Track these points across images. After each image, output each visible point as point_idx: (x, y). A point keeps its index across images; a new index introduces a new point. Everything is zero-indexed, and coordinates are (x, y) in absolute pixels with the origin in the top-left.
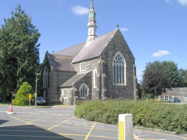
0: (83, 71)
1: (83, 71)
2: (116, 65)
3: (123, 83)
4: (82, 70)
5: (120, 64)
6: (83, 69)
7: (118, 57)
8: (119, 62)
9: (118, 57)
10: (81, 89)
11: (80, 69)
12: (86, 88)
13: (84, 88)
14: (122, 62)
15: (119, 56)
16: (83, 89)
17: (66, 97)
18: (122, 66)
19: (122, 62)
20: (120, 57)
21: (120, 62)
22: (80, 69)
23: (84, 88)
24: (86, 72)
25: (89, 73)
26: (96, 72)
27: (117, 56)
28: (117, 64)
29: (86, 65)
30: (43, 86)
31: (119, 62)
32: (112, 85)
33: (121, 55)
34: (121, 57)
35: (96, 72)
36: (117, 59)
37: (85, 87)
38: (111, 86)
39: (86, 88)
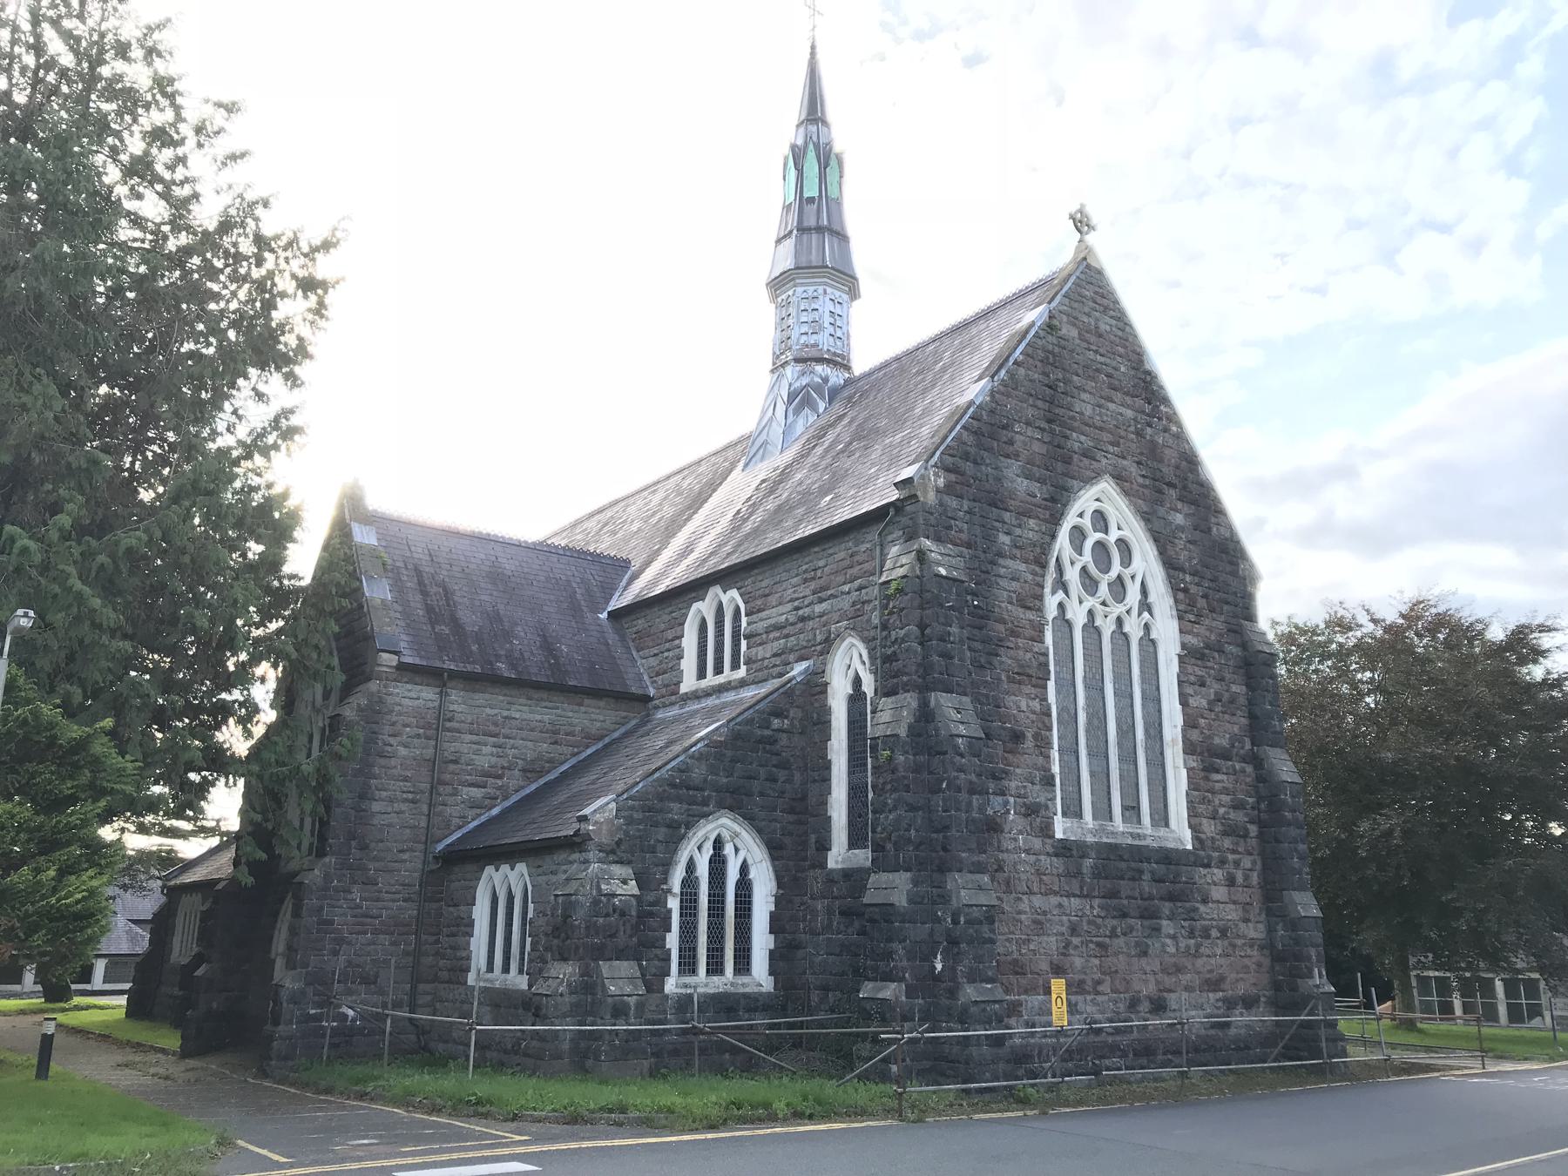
0: (721, 679)
1: (711, 680)
2: (1078, 616)
3: (743, 962)
4: (701, 674)
5: (1118, 609)
6: (719, 670)
7: (1093, 537)
8: (1103, 589)
9: (1093, 537)
10: (690, 882)
11: (689, 664)
12: (744, 869)
13: (718, 864)
14: (1133, 595)
15: (1101, 520)
16: (703, 870)
17: (506, 969)
18: (1133, 628)
19: (1133, 595)
20: (1114, 535)
21: (1118, 588)
22: (689, 664)
23: (718, 864)
24: (750, 693)
25: (775, 708)
26: (857, 682)
27: (1087, 522)
28: (1090, 602)
29: (744, 620)
30: (824, 846)
31: (1103, 589)
32: (1046, 830)
33: (1126, 522)
34: (1126, 533)
35: (857, 682)
36: (1087, 557)
37: (728, 849)
38: (1037, 843)
39: (744, 869)
